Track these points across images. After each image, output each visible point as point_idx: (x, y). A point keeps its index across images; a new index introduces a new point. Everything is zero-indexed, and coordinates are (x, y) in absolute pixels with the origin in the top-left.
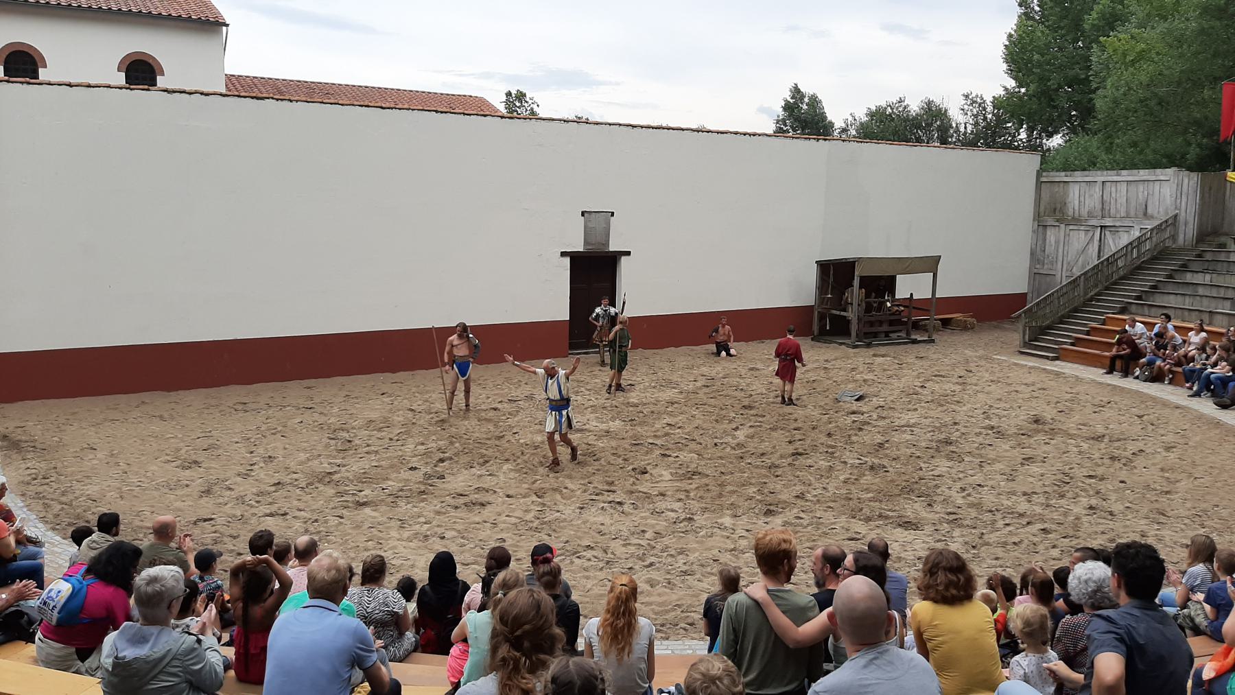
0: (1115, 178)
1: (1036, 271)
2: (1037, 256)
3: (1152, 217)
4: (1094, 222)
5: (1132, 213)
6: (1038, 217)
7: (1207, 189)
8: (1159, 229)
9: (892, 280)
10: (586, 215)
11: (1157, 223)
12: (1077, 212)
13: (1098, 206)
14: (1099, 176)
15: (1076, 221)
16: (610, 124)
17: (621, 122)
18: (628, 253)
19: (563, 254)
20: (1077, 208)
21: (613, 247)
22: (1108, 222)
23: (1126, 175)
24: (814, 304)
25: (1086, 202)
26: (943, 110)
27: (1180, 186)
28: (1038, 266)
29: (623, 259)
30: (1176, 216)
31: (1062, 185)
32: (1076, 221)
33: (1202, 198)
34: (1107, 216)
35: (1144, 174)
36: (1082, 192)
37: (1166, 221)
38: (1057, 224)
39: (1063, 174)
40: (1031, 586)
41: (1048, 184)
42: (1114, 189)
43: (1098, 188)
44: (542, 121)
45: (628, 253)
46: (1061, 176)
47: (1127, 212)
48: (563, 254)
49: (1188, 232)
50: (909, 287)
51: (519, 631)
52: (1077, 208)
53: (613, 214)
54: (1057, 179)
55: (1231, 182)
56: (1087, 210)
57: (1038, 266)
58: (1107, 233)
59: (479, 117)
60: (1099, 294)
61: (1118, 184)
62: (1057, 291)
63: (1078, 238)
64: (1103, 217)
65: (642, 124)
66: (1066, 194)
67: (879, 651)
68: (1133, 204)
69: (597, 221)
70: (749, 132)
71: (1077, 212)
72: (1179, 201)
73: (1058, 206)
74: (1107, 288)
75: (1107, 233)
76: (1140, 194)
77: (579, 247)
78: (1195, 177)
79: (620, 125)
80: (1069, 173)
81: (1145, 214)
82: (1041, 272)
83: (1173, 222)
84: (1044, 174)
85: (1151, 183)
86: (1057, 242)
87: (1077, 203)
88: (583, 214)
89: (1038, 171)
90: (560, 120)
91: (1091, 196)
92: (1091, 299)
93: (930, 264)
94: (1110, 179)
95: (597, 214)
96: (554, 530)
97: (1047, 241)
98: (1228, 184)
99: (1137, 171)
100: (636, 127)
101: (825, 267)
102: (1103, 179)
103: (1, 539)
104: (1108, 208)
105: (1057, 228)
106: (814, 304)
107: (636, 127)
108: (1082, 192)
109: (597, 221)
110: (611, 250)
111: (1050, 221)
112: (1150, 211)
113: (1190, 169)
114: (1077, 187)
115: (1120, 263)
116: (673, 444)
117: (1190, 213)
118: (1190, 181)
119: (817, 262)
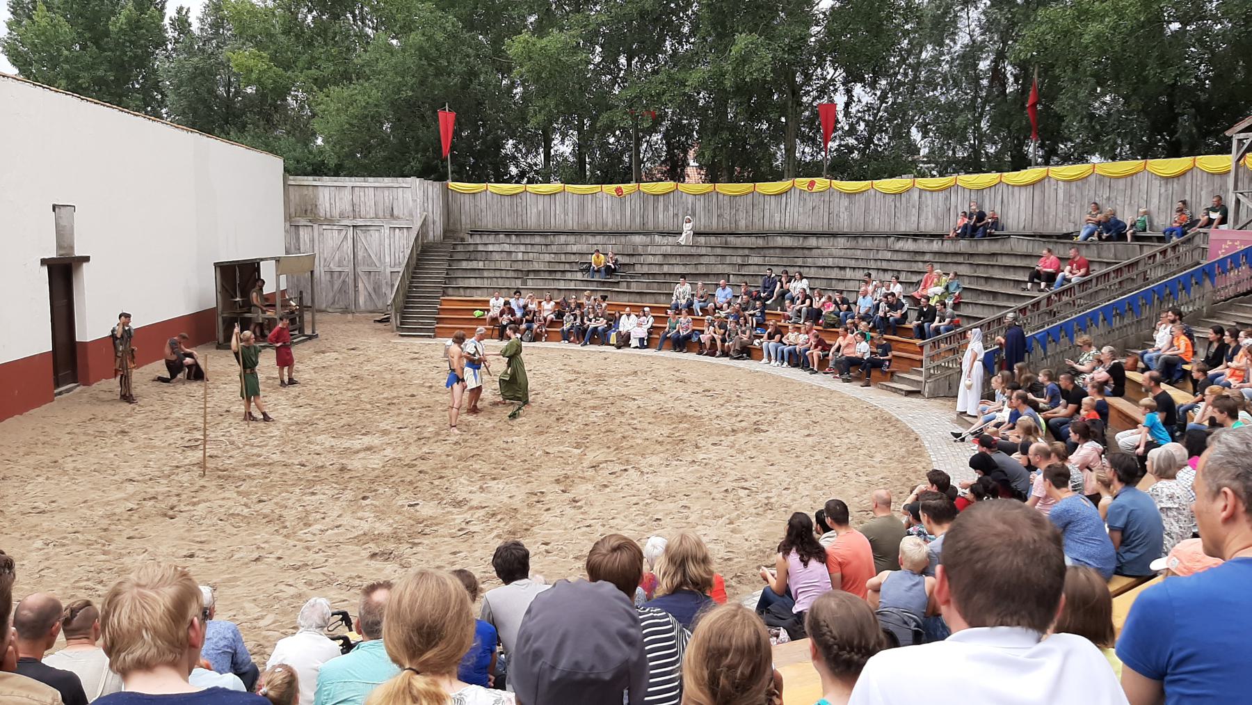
0: (315, 183)
3: (398, 218)
5: (381, 214)
6: (288, 217)
15: (330, 221)
20: (328, 210)
22: (359, 222)
27: (426, 193)
31: (311, 188)
32: (330, 221)
34: (967, 192)
35: (387, 181)
36: (333, 195)
42: (362, 194)
43: (347, 192)
52: (328, 210)
56: (338, 210)
64: (354, 218)
66: (316, 198)
73: (309, 208)
81: (392, 215)
86: (312, 241)
87: (328, 205)
94: (358, 184)
97: (301, 240)
105: (310, 228)
108: (333, 195)
111: (302, 222)
112: (395, 213)
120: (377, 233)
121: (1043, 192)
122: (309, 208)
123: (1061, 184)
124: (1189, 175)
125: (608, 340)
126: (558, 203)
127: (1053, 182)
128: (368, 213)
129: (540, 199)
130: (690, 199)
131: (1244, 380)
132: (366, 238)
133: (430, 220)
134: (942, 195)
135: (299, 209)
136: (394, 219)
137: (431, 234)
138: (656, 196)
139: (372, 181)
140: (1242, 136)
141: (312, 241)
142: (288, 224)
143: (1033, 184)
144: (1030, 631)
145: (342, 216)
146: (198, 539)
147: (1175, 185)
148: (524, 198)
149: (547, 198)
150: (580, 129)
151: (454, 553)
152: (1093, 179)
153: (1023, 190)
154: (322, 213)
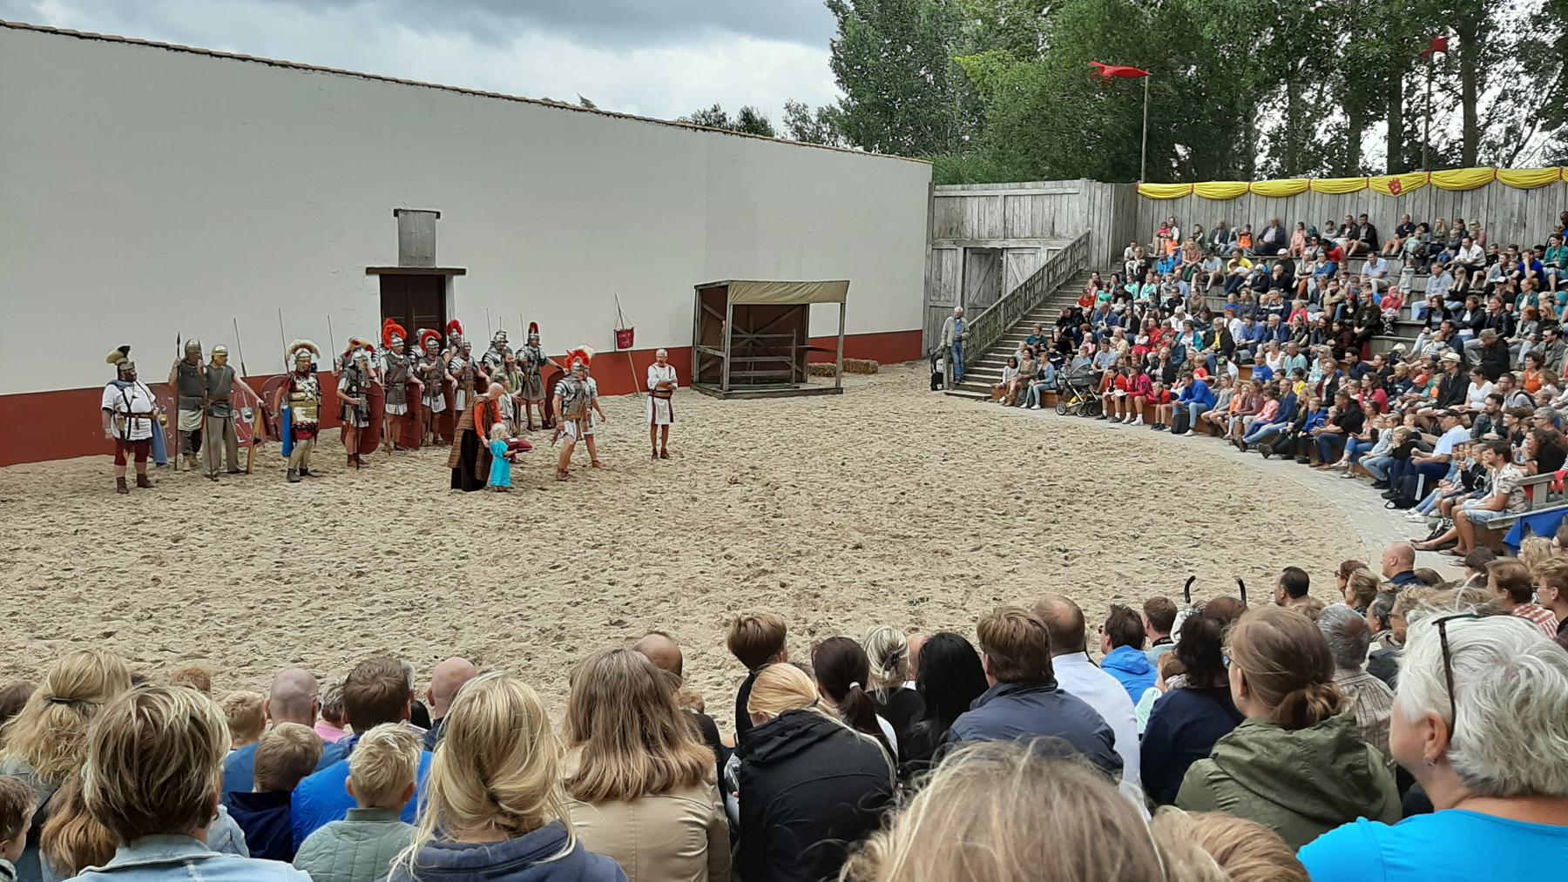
0: (1019, 192)
1: (931, 303)
3: (1060, 236)
5: (1038, 234)
6: (932, 239)
7: (1120, 203)
9: (803, 310)
10: (400, 215)
11: (1067, 243)
12: (976, 236)
13: (1000, 225)
14: (1001, 189)
16: (430, 86)
17: (445, 85)
18: (462, 272)
19: (370, 271)
20: (976, 227)
21: (440, 263)
24: (691, 345)
25: (987, 221)
26: (837, 107)
27: (1092, 199)
28: (933, 298)
30: (1088, 234)
31: (958, 200)
33: (1116, 212)
35: (1050, 186)
36: (982, 207)
37: (1079, 240)
38: (954, 247)
39: (959, 187)
41: (943, 199)
42: (1017, 204)
43: (999, 203)
44: (331, 74)
45: (462, 272)
46: (956, 190)
47: (1033, 232)
48: (370, 271)
49: (1101, 252)
51: (1345, 451)
52: (976, 227)
53: (438, 215)
54: (953, 194)
55: (1143, 196)
56: (987, 229)
57: (933, 298)
58: (1010, 256)
59: (235, 61)
60: (1018, 324)
61: (1022, 199)
62: (978, 321)
64: (1005, 238)
65: (474, 90)
66: (963, 212)
68: (1038, 222)
70: (613, 111)
71: (976, 236)
72: (1091, 217)
73: (955, 225)
74: (1025, 317)
75: (1010, 256)
76: (1046, 210)
77: (392, 261)
78: (1107, 186)
79: (444, 88)
80: (966, 186)
81: (1052, 233)
82: (938, 304)
83: (1085, 241)
84: (938, 187)
85: (1059, 197)
87: (976, 222)
88: (396, 213)
89: (930, 184)
90: (358, 75)
91: (991, 213)
92: (1011, 330)
93: (838, 292)
94: (1013, 192)
95: (417, 214)
96: (883, 479)
97: (944, 267)
98: (1140, 197)
99: (1042, 183)
100: (465, 92)
101: (619, 333)
102: (1005, 192)
104: (1010, 227)
105: (954, 252)
106: (691, 345)
107: (465, 92)
108: (982, 207)
110: (438, 267)
111: (946, 244)
112: (1057, 230)
113: (1101, 178)
114: (976, 201)
115: (1038, 288)
117: (1104, 228)
118: (1103, 193)
119: (696, 287)
120: (1032, 258)
122: (955, 225)
126: (1297, 208)
128: (1022, 231)
129: (1272, 203)
131: (1566, 433)
132: (1018, 266)
133: (1095, 237)
135: (944, 227)
136: (1055, 239)
137: (1095, 258)
138: (1461, 191)
139: (1030, 187)
142: (930, 247)
148: (1246, 203)
149: (1209, 202)
150: (1429, 102)
151: (108, 635)
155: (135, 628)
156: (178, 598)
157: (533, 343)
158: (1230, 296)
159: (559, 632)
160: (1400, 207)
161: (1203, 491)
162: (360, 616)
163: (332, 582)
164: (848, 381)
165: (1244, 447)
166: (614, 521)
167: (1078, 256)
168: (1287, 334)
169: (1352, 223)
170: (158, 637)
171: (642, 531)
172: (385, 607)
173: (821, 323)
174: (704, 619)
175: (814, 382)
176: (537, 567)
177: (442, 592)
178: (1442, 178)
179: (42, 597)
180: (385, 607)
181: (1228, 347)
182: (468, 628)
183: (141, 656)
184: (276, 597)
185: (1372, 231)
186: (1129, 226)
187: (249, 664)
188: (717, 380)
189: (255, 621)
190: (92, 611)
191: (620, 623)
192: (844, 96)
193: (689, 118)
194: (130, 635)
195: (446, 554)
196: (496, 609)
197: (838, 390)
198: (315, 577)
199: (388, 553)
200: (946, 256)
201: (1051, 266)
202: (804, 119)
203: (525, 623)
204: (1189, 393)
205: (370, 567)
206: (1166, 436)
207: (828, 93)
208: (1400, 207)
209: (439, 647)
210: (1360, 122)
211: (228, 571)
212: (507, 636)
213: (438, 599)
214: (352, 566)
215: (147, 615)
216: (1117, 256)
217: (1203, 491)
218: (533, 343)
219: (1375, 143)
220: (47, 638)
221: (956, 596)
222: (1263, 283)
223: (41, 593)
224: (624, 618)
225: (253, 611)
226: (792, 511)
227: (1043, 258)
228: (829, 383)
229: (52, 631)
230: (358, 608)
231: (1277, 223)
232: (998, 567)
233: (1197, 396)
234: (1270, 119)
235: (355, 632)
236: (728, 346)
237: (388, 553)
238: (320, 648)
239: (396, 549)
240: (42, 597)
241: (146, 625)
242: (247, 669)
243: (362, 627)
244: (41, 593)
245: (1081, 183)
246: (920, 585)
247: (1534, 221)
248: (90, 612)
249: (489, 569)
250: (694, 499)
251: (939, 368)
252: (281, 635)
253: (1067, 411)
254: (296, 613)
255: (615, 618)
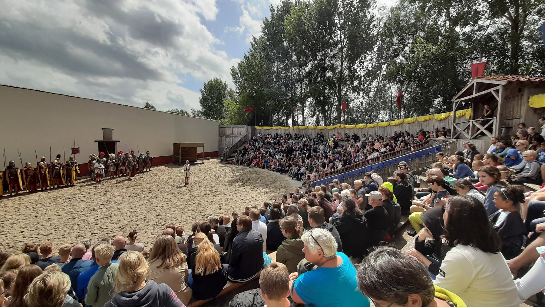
2: (220, 143)
4: (231, 136)
6: (219, 135)
8: (244, 137)
11: (243, 136)
13: (232, 133)
15: (228, 136)
18: (119, 141)
19: (96, 141)
22: (233, 136)
23: (237, 126)
27: (247, 129)
29: (118, 143)
30: (247, 135)
32: (228, 136)
34: (380, 127)
40: (310, 218)
45: (119, 141)
48: (96, 141)
49: (249, 138)
50: (199, 150)
53: (113, 130)
63: (228, 139)
67: (331, 194)
69: (107, 132)
78: (250, 127)
86: (224, 140)
93: (202, 145)
103: (543, 64)
109: (107, 132)
115: (239, 144)
116: (74, 242)
121: (402, 127)
123: (407, 124)
124: (447, 119)
125: (527, 235)
127: (405, 124)
130: (311, 130)
134: (374, 129)
140: (457, 101)
141: (224, 140)
143: (399, 125)
144: (22, 18)
145: (230, 135)
146: (94, 235)
147: (443, 123)
152: (416, 122)
153: (396, 127)
154: (226, 134)
155: (31, 229)
156: (42, 220)
157: (148, 154)
158: (270, 145)
159: (144, 219)
160: (294, 131)
161: (268, 179)
162: (95, 220)
163: (86, 213)
164: (205, 161)
165: (273, 171)
166: (156, 193)
167: (245, 138)
168: (279, 152)
169: (288, 134)
170: (37, 231)
171: (163, 195)
172: (101, 217)
173: (199, 150)
174: (177, 212)
175: (198, 162)
176: (139, 204)
177: (115, 212)
178: (300, 127)
179: (3, 224)
180: (101, 217)
181: (270, 154)
182: (122, 220)
183: (32, 236)
184: (71, 218)
185: (291, 135)
186: (253, 133)
187: (64, 235)
188: (178, 162)
189: (65, 224)
190: (17, 227)
191: (159, 215)
192: (202, 108)
193: (171, 111)
194: (29, 231)
195: (116, 203)
196: (129, 215)
197: (203, 163)
198: (82, 212)
199: (102, 204)
200: (222, 138)
201: (241, 140)
202: (195, 111)
203: (136, 217)
204: (265, 162)
205: (97, 208)
206: (261, 169)
207: (199, 107)
208: (294, 131)
209: (116, 225)
210: (287, 119)
211: (57, 212)
212: (132, 221)
213: (114, 214)
214: (91, 208)
215: (33, 226)
216: (252, 138)
217: (268, 179)
218: (148, 154)
219: (290, 121)
220: (5, 234)
221: (227, 202)
222: (275, 144)
223: (3, 222)
224: (160, 214)
225: (65, 222)
226: (195, 188)
227: (239, 139)
228: (201, 162)
229: (6, 232)
230: (94, 218)
231: (276, 133)
232: (235, 196)
233: (266, 162)
234: (275, 117)
235: (93, 224)
236: (180, 155)
237: (102, 204)
238: (84, 229)
239: (103, 203)
240: (3, 224)
241: (34, 228)
242: (63, 236)
243: (33, 240)
244: (3, 222)
245: (245, 126)
246: (221, 201)
247: (313, 134)
248: (17, 226)
249: (127, 206)
250: (174, 187)
251: (222, 158)
252: (72, 227)
253: (245, 166)
254: (77, 220)
255: (158, 214)
